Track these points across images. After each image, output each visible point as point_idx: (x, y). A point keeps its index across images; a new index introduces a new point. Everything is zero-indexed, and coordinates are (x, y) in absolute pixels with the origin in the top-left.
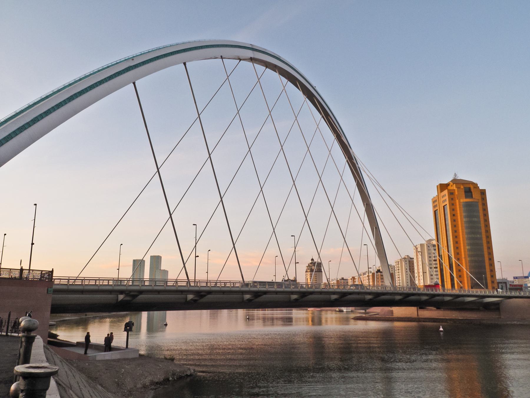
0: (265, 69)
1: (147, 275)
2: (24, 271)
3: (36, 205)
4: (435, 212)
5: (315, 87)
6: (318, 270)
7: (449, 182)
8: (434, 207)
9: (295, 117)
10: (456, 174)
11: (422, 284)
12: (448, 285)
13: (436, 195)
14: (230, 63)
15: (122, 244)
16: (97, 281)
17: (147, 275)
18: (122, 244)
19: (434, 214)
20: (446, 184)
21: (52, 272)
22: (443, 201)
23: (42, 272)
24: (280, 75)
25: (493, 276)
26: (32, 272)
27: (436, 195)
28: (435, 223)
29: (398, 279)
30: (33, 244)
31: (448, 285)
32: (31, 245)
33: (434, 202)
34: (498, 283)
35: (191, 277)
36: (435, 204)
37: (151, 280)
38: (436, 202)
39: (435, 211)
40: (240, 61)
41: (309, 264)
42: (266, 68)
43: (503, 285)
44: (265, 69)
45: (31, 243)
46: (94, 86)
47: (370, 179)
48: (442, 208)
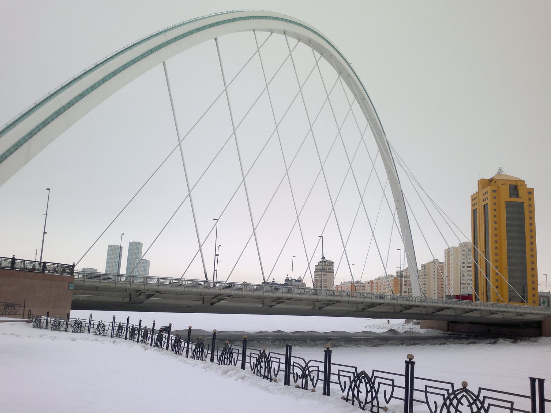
0: (298, 43)
1: (123, 271)
2: (47, 265)
3: (48, 189)
4: (474, 212)
5: (351, 64)
6: (330, 271)
7: (492, 178)
8: (473, 205)
9: (330, 98)
10: (502, 168)
11: (42, 318)
12: (482, 295)
13: (477, 192)
14: (262, 36)
15: (123, 234)
16: (80, 275)
17: (123, 271)
18: (123, 234)
19: (473, 225)
20: (489, 179)
21: (73, 266)
22: (484, 199)
23: (58, 265)
24: (379, 151)
25: (535, 288)
26: (54, 265)
27: (477, 192)
28: (473, 238)
29: (424, 286)
30: (45, 233)
31: (482, 295)
32: (43, 234)
33: (473, 199)
34: (540, 296)
35: (210, 278)
36: (475, 202)
37: (127, 276)
38: (476, 206)
39: (474, 210)
40: (271, 34)
41: (318, 263)
42: (299, 41)
43: (545, 300)
44: (298, 43)
45: (43, 232)
46: (126, 65)
47: (400, 163)
48: (483, 207)
